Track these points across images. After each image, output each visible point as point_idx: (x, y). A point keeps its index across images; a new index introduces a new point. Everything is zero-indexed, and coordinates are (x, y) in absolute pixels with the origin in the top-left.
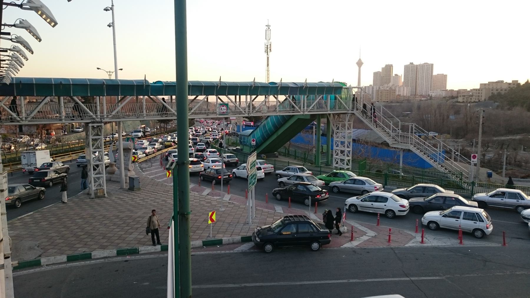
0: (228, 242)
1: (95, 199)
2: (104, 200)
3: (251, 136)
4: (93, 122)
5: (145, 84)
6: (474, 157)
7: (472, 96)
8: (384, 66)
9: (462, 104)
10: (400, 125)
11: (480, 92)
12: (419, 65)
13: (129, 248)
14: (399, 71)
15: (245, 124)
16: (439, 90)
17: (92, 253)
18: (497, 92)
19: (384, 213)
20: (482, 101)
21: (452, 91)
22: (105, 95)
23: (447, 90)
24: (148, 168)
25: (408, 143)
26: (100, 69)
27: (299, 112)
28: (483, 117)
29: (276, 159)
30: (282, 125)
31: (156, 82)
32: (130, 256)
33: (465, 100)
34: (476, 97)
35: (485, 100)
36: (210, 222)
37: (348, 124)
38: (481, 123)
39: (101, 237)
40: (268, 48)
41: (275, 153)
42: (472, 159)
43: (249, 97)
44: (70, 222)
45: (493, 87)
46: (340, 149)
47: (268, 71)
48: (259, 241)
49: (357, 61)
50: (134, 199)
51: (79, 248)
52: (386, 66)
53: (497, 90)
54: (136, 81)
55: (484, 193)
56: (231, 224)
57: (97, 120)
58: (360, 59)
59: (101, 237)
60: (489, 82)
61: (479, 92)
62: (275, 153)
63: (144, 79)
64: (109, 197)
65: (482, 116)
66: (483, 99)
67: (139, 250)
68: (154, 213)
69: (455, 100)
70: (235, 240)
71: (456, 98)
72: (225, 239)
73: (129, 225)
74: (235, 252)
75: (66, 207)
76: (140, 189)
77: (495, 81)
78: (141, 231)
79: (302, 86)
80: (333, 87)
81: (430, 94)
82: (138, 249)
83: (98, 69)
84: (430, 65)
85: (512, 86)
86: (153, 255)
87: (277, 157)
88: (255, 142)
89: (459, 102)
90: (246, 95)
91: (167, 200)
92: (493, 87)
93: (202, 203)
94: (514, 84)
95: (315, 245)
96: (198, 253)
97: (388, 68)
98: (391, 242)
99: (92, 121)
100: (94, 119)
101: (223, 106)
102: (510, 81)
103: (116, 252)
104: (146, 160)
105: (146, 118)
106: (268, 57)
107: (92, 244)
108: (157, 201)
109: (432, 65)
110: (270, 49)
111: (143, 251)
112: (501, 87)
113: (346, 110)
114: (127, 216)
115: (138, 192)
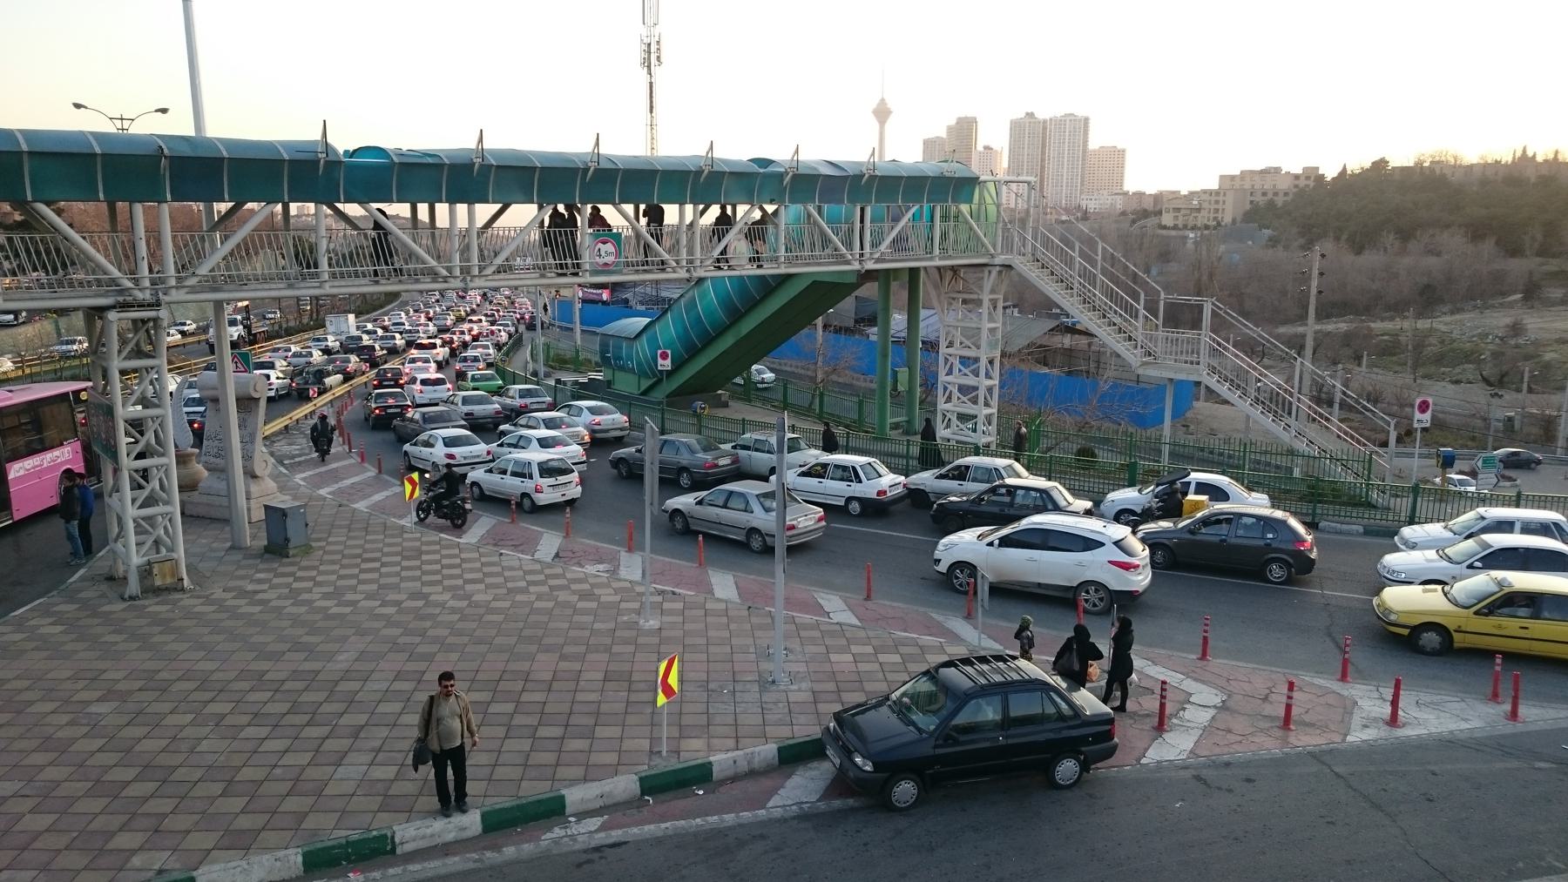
0: (730, 773)
1: (146, 602)
2: (182, 603)
3: (644, 338)
4: (124, 306)
5: (324, 155)
6: (1424, 406)
7: (1199, 210)
8: (953, 122)
9: (1173, 233)
10: (1162, 303)
11: (1221, 198)
12: (1051, 119)
13: (355, 836)
14: (994, 137)
15: (580, 294)
16: (1105, 192)
17: (195, 874)
18: (1266, 198)
19: (842, 504)
20: (1226, 225)
21: (1140, 195)
22: (169, 197)
23: (1126, 194)
24: (300, 456)
25: (1198, 363)
26: (86, 108)
27: (848, 263)
28: (1321, 274)
29: (721, 413)
30: (753, 304)
31: (355, 151)
32: (363, 872)
33: (1180, 223)
34: (1209, 212)
35: (1234, 221)
36: (661, 699)
37: (991, 300)
38: (1314, 291)
39: (217, 788)
40: (649, 53)
41: (720, 392)
42: (1418, 415)
43: (689, 208)
44: (65, 719)
45: (1253, 186)
46: (955, 380)
47: (652, 129)
48: (868, 768)
49: (875, 106)
50: (300, 591)
51: (134, 852)
52: (960, 121)
53: (1264, 194)
54: (286, 144)
55: (1437, 524)
56: (712, 686)
57: (140, 295)
58: (883, 100)
59: (217, 788)
60: (1242, 172)
61: (1217, 198)
62: (720, 392)
63: (318, 137)
64: (198, 588)
65: (1317, 272)
66: (1228, 219)
67: (397, 840)
68: (446, 687)
69: (1151, 222)
70: (757, 759)
71: (1155, 216)
72: (722, 760)
73: (317, 717)
74: (778, 813)
75: (34, 644)
76: (311, 547)
77: (1259, 169)
78: (377, 743)
79: (857, 172)
80: (951, 179)
81: (1084, 204)
82: (393, 837)
83: (78, 106)
84: (1080, 120)
85: (1302, 183)
86: (456, 859)
87: (726, 405)
88: (669, 360)
89: (1165, 227)
90: (682, 204)
91: (430, 594)
92: (1253, 186)
93: (563, 596)
94: (1308, 178)
95: (1067, 768)
96: (635, 830)
97: (965, 129)
98: (1292, 727)
99: (119, 303)
100: (122, 291)
101: (604, 243)
102: (1297, 169)
103: (300, 859)
104: (286, 427)
105: (331, 287)
106: (651, 84)
107: (183, 828)
108: (392, 597)
109: (1086, 120)
110: (658, 58)
111: (414, 840)
112: (1274, 186)
113: (983, 256)
114: (296, 675)
115: (304, 563)
